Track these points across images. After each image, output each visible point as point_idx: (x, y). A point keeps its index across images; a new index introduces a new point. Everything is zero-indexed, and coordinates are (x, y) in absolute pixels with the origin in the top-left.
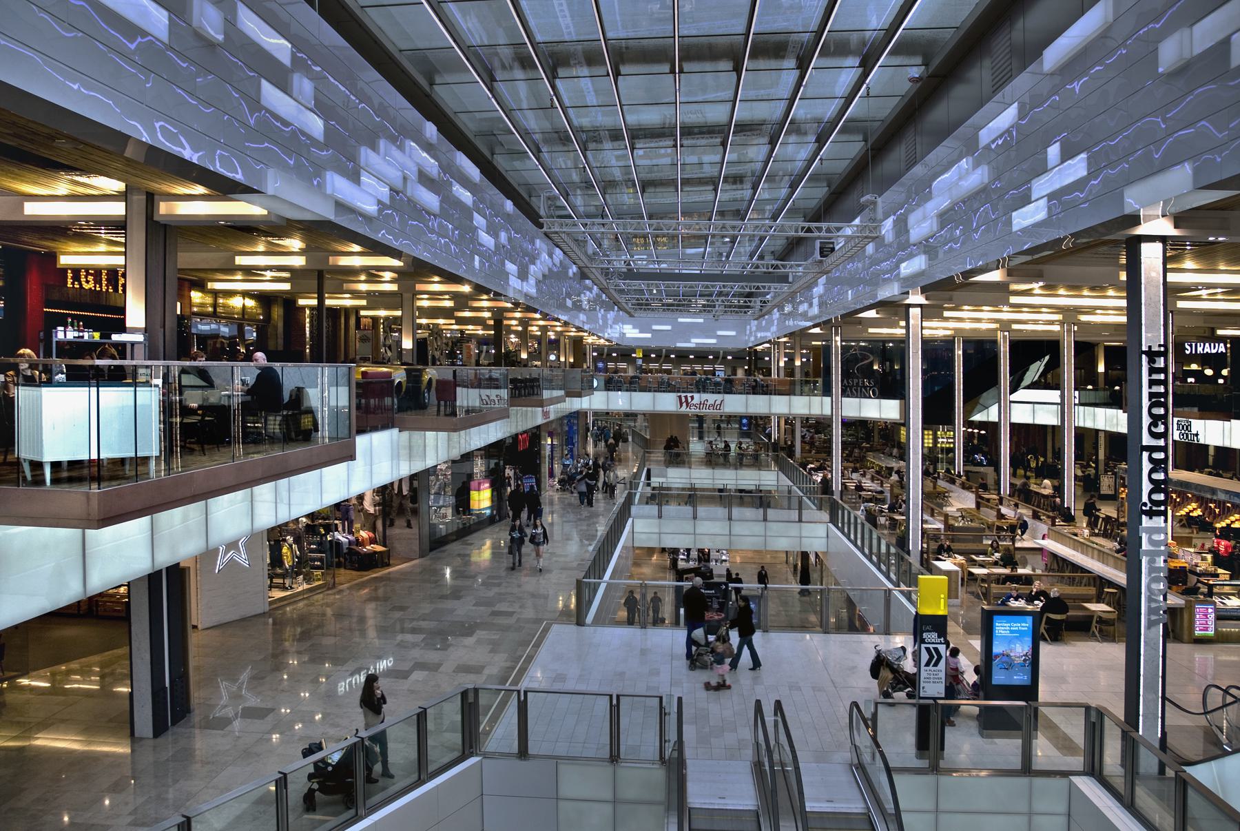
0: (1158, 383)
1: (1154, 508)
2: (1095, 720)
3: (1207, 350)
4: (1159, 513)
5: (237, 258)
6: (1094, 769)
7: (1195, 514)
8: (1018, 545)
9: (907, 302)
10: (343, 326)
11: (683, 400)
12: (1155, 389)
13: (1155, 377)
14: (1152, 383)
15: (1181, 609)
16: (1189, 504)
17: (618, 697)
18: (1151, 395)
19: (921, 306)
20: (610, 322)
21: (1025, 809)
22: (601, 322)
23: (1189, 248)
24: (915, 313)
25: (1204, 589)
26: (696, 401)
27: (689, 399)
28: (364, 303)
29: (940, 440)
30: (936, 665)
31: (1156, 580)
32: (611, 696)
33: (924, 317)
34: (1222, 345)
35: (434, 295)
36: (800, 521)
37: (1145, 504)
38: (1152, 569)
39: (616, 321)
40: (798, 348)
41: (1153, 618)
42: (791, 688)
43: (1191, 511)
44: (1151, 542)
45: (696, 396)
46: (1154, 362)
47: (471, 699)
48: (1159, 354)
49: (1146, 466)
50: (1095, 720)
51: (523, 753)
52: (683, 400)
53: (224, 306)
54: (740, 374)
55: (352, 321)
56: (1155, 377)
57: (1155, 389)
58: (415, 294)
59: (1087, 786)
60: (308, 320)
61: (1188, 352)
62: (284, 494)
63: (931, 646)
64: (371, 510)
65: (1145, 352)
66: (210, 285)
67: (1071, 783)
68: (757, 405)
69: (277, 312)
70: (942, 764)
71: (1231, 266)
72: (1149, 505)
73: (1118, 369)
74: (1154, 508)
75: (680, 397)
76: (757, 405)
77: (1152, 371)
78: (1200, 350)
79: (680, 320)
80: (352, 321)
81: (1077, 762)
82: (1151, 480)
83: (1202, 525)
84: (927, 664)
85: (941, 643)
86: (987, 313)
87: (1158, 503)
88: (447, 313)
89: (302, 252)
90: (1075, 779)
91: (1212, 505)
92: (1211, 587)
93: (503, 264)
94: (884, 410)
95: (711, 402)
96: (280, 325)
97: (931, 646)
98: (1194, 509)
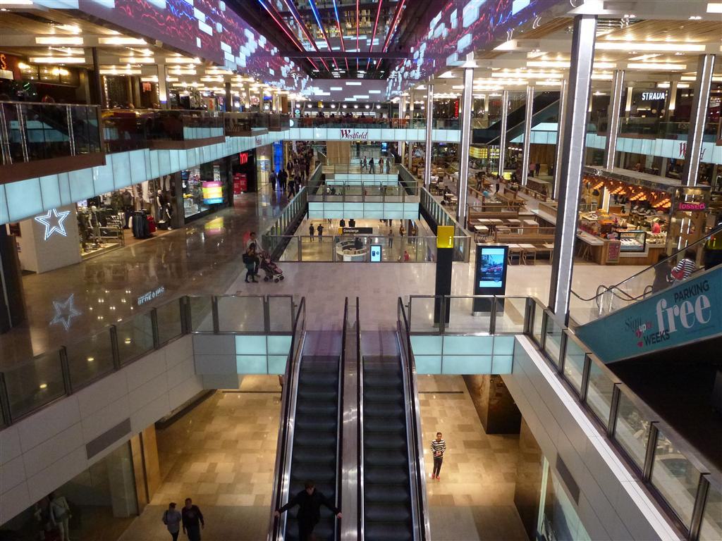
2: (531, 304)
3: (654, 98)
5: (37, 38)
6: (528, 333)
7: (642, 199)
8: (520, 213)
9: (464, 66)
10: (131, 89)
11: (344, 132)
15: (602, 246)
16: (664, 199)
17: (268, 297)
20: (303, 85)
21: (491, 354)
22: (296, 85)
23: (610, 25)
24: (469, 73)
25: (616, 235)
26: (352, 133)
27: (348, 132)
28: (177, 80)
29: (492, 154)
32: (264, 297)
33: (474, 77)
34: (663, 94)
35: (212, 76)
36: (403, 202)
39: (308, 85)
40: (412, 101)
42: (374, 292)
43: (664, 204)
45: (352, 130)
47: (185, 302)
50: (531, 304)
51: (216, 331)
52: (344, 132)
53: (48, 75)
54: (385, 116)
55: (137, 85)
58: (168, 66)
59: (524, 341)
60: (106, 85)
61: (643, 99)
62: (64, 185)
64: (148, 201)
66: (31, 60)
67: (515, 339)
68: (388, 135)
69: (83, 77)
70: (446, 330)
71: (657, 37)
73: (588, 109)
75: (342, 131)
76: (388, 135)
78: (650, 98)
79: (348, 84)
80: (137, 85)
81: (521, 327)
83: (625, 200)
86: (518, 73)
88: (188, 78)
89: (80, 35)
90: (517, 336)
91: (631, 188)
92: (619, 233)
93: (220, 45)
94: (452, 136)
95: (360, 134)
96: (87, 88)
98: (666, 203)
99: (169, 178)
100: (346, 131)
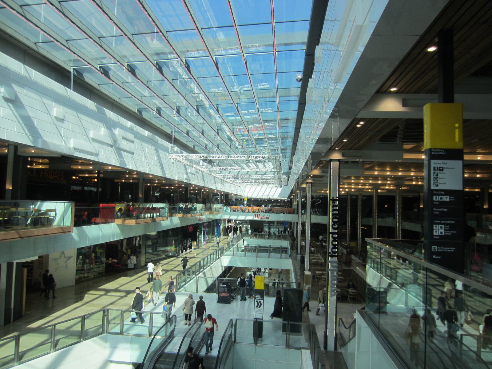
0: (336, 210)
1: (333, 254)
4: (335, 256)
11: (256, 215)
12: (335, 212)
13: (335, 208)
14: (334, 210)
18: (333, 215)
19: (311, 183)
27: (258, 215)
30: (260, 307)
31: (334, 280)
37: (330, 253)
38: (332, 276)
41: (333, 293)
44: (332, 266)
46: (334, 203)
48: (336, 200)
49: (331, 239)
56: (335, 208)
57: (335, 212)
63: (258, 300)
65: (331, 200)
72: (332, 253)
74: (333, 254)
77: (334, 206)
82: (332, 244)
84: (257, 307)
85: (261, 299)
87: (335, 252)
97: (258, 300)
99: (138, 238)
100: (257, 214)
